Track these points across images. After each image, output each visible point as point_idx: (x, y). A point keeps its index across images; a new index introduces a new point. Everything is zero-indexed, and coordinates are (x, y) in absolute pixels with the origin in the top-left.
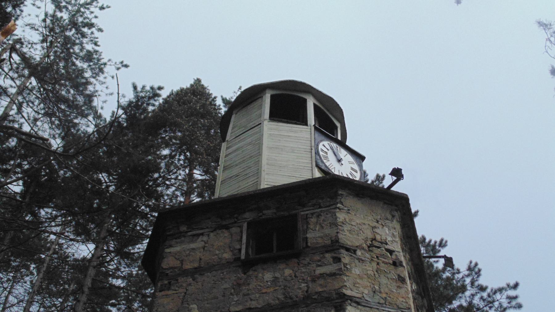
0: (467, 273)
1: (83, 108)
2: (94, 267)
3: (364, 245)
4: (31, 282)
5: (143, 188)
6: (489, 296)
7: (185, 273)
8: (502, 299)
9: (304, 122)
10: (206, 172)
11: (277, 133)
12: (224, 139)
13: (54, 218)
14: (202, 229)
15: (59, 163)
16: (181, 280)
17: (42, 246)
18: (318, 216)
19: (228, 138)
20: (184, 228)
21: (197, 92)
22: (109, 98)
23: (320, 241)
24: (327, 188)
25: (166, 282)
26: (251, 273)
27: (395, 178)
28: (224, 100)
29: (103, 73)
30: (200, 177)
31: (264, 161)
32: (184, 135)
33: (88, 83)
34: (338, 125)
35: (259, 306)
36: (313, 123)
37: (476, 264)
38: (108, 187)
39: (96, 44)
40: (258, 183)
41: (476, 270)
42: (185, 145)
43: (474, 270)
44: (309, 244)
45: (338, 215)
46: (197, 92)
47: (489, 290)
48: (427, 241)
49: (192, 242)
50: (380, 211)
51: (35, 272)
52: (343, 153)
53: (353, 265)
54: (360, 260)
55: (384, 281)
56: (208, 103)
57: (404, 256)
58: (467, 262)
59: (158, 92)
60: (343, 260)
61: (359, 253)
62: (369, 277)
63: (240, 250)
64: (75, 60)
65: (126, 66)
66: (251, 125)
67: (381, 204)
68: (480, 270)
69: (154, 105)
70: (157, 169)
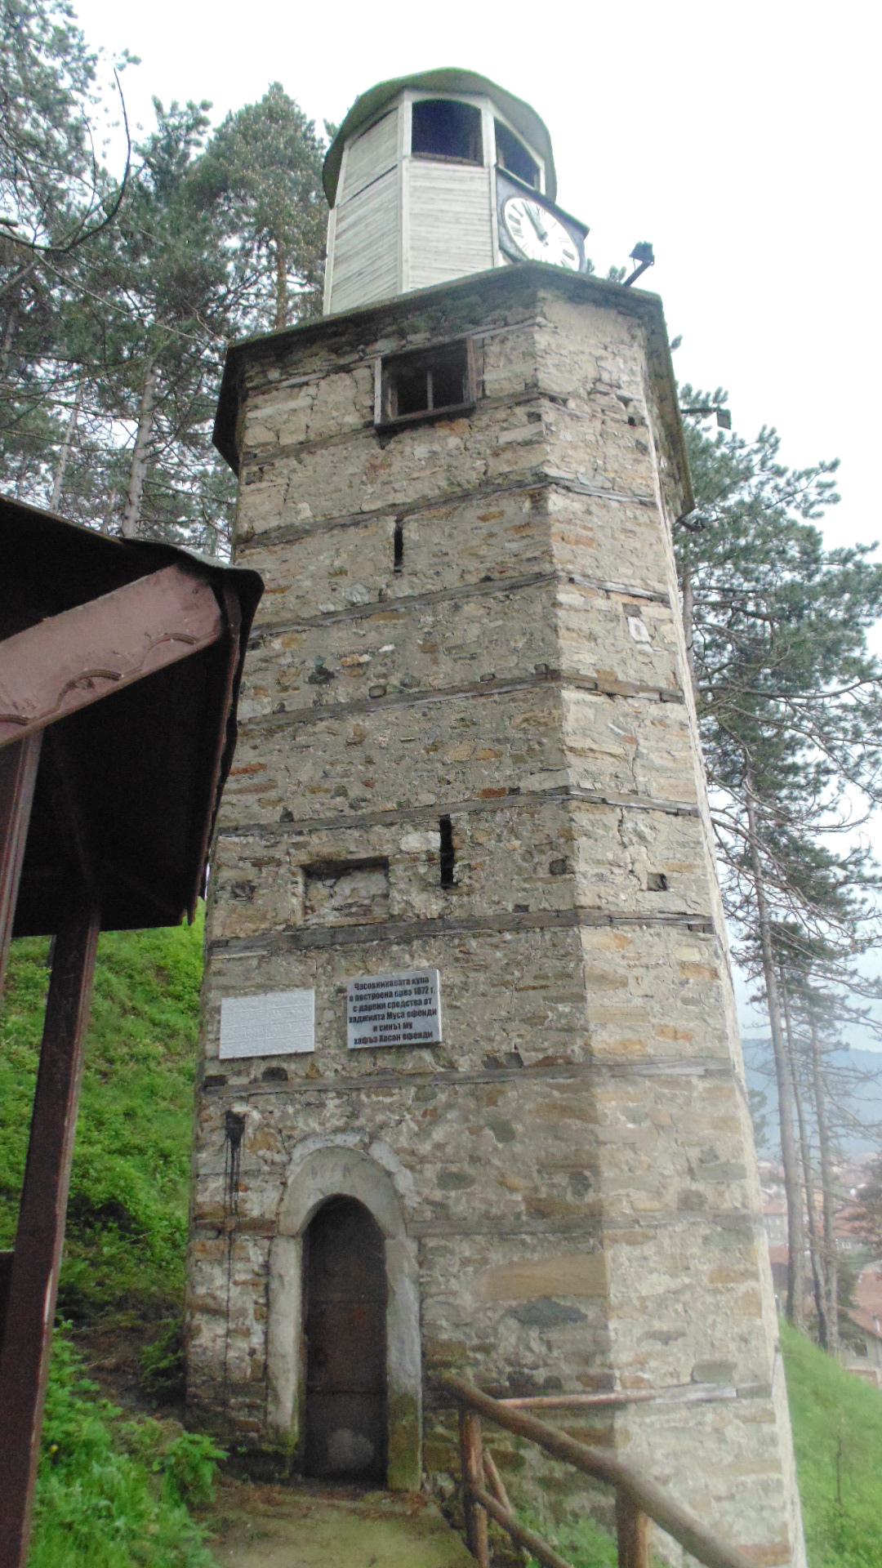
0: (756, 446)
1: (70, 158)
2: (143, 461)
3: (581, 390)
4: (47, 493)
5: (203, 314)
6: (788, 484)
7: (284, 452)
8: (808, 487)
9: (477, 158)
10: (310, 279)
11: (427, 184)
12: (331, 205)
13: (61, 380)
14: (305, 374)
15: (48, 273)
16: (278, 463)
17: (52, 432)
18: (502, 342)
19: (338, 200)
20: (274, 375)
21: (276, 112)
22: (114, 139)
23: (506, 385)
24: (515, 288)
25: (255, 469)
26: (392, 446)
27: (639, 263)
28: (329, 128)
29: (93, 77)
30: (298, 289)
31: (407, 254)
32: (261, 205)
33: (66, 100)
34: (540, 163)
35: (409, 501)
36: (494, 161)
37: (773, 432)
38: (142, 316)
39: (69, 13)
40: (397, 284)
41: (772, 440)
42: (267, 225)
43: (768, 441)
44: (488, 393)
45: (537, 337)
46: (276, 112)
47: (789, 475)
48: (694, 393)
49: (291, 397)
50: (611, 327)
51: (49, 477)
52: (547, 220)
53: (562, 425)
54: (574, 417)
55: (612, 451)
56: (299, 134)
57: (650, 411)
58: (759, 430)
59: (203, 113)
60: (544, 417)
61: (572, 404)
62: (587, 444)
63: (372, 408)
64: (35, 53)
65: (136, 61)
66: (379, 170)
67: (613, 313)
68: (777, 441)
69: (198, 144)
70: (222, 278)
